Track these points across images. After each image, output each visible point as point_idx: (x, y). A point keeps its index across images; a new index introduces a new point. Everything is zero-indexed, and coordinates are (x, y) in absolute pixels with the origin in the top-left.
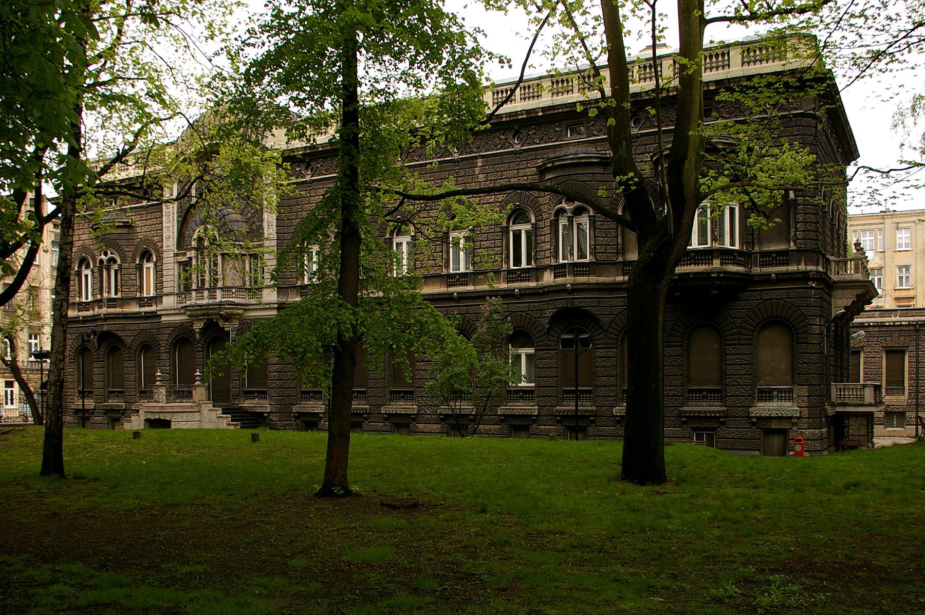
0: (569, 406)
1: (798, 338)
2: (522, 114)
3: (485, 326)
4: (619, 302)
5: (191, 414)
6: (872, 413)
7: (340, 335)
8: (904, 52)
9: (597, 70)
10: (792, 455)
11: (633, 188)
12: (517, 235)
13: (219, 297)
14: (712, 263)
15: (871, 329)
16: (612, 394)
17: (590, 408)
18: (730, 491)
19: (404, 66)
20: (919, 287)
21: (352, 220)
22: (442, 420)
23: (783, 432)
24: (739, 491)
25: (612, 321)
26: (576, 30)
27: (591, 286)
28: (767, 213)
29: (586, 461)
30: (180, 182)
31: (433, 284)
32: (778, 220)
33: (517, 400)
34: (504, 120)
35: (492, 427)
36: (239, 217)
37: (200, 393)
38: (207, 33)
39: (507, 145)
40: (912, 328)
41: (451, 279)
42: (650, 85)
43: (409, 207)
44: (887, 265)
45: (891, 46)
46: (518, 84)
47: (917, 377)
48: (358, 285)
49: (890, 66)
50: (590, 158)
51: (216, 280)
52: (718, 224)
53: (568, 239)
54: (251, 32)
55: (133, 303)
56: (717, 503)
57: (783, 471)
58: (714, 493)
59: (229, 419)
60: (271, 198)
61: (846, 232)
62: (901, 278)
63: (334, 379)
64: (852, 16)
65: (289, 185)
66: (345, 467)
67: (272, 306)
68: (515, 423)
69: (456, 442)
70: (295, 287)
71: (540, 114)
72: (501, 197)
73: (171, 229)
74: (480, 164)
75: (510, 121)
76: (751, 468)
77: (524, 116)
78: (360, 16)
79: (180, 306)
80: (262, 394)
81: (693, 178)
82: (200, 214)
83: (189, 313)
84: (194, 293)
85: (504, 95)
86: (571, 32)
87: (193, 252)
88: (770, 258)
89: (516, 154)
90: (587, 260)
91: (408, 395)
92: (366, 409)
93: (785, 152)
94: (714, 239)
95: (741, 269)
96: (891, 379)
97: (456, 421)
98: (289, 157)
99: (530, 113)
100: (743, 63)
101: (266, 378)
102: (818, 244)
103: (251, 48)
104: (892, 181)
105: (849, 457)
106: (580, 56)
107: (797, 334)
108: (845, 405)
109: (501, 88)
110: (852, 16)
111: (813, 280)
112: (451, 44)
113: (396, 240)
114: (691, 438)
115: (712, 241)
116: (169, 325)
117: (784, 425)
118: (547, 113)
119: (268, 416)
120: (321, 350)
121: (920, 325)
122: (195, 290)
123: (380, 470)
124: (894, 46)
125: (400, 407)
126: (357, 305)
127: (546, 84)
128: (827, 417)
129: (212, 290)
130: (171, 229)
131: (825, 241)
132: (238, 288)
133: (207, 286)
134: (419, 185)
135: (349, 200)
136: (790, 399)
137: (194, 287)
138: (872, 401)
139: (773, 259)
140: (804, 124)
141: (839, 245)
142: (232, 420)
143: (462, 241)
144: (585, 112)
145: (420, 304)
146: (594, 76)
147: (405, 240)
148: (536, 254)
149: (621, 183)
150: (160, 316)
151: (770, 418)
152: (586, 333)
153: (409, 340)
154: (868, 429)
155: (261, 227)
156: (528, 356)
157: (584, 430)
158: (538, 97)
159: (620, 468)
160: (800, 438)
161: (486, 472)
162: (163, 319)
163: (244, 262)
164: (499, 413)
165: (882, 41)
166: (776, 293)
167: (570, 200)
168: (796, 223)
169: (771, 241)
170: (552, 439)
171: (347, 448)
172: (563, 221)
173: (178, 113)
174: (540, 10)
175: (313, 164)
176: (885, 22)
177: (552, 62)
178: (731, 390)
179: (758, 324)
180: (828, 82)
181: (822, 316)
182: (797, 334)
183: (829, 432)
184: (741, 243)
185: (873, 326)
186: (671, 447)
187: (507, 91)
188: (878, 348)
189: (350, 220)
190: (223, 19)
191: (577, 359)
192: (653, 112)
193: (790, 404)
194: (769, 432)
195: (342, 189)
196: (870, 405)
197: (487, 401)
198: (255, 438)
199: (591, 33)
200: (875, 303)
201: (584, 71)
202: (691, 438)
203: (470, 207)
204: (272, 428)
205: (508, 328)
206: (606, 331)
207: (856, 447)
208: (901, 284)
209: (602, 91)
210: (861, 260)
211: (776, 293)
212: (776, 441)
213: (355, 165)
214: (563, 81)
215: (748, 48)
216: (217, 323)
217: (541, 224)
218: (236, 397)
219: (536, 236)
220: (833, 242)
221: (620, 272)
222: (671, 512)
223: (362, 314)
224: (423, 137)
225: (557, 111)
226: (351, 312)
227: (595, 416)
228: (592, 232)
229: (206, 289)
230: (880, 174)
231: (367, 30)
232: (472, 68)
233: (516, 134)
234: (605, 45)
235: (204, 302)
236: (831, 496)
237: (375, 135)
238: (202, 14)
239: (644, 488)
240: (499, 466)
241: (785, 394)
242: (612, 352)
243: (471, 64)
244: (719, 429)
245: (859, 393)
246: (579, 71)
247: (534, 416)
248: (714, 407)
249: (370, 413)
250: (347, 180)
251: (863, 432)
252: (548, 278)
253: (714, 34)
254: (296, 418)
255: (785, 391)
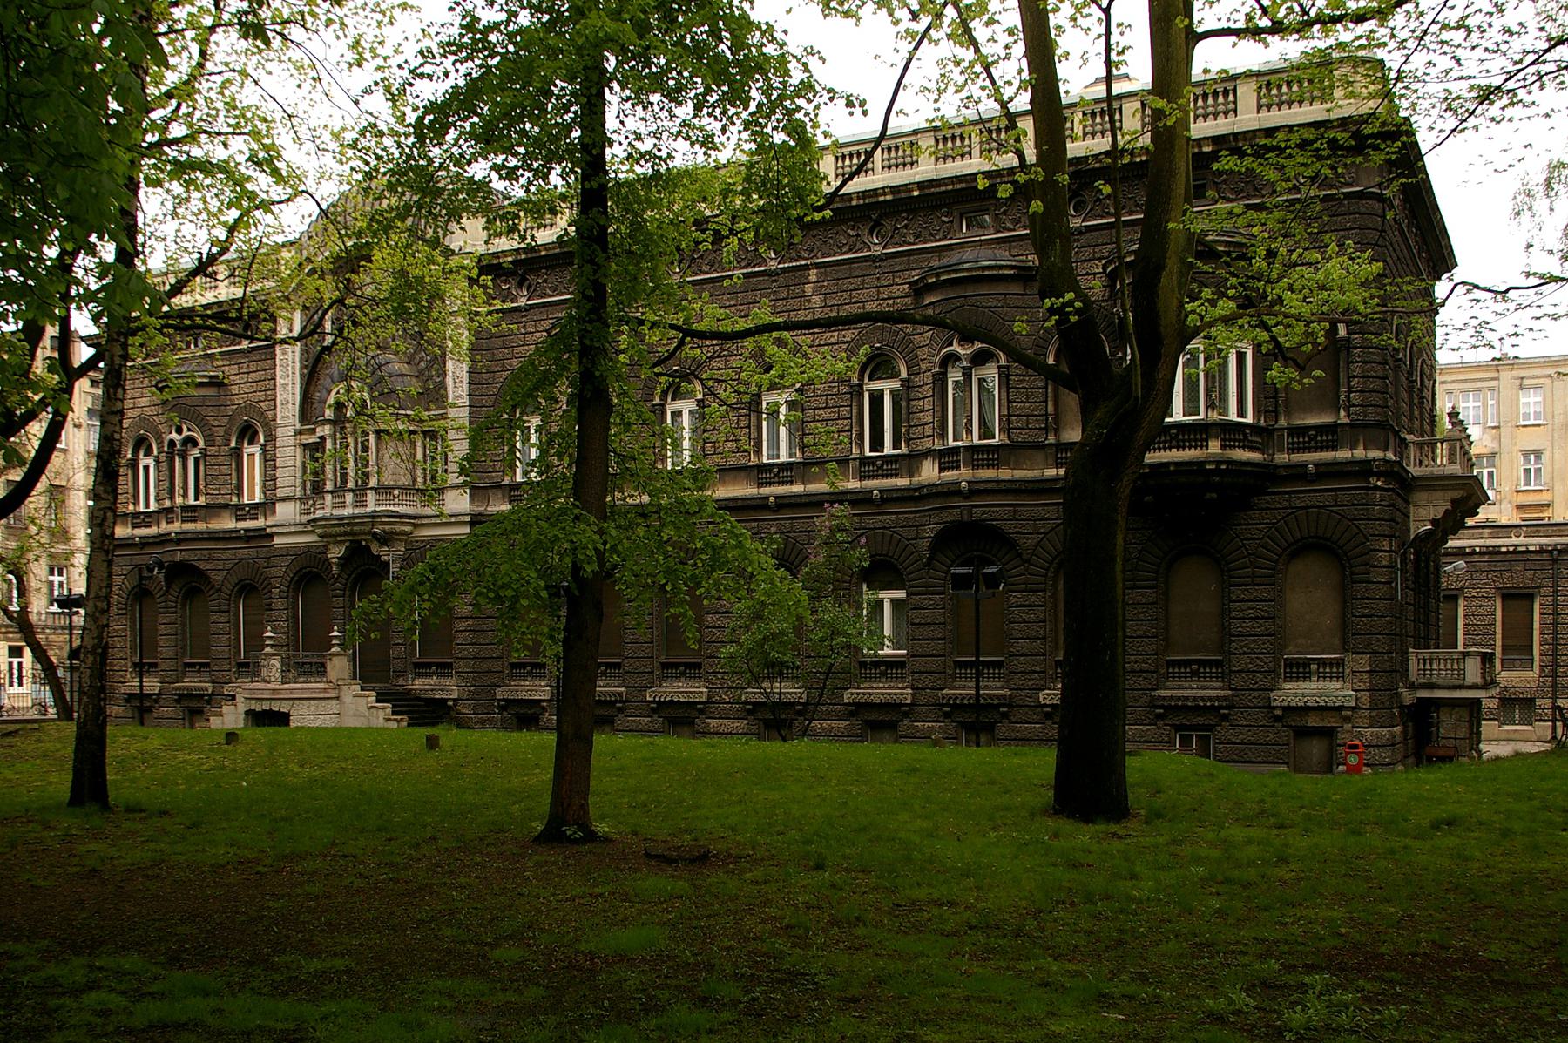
0: (964, 689)
1: (1352, 573)
2: (885, 194)
3: (823, 552)
4: (1049, 512)
5: (323, 703)
6: (1478, 701)
7: (576, 569)
8: (1532, 87)
9: (1012, 118)
10: (1343, 772)
11: (1073, 319)
12: (877, 399)
13: (372, 503)
14: (1207, 447)
15: (1476, 558)
16: (1037, 669)
17: (1000, 692)
18: (1237, 833)
19: (685, 111)
20: (1558, 487)
21: (597, 374)
22: (750, 712)
23: (1328, 733)
24: (1253, 832)
25: (1038, 544)
26: (977, 50)
27: (1002, 486)
28: (1300, 362)
29: (993, 782)
30: (305, 308)
31: (734, 481)
32: (1318, 373)
33: (876, 678)
34: (854, 203)
35: (833, 724)
36: (404, 368)
37: (338, 666)
38: (351, 56)
39: (859, 245)
40: (1545, 556)
41: (765, 474)
42: (1102, 144)
43: (693, 351)
44: (1504, 450)
45: (1510, 78)
46: (877, 142)
47: (1555, 639)
48: (607, 483)
49: (1509, 112)
50: (1001, 267)
51: (367, 475)
52: (1217, 380)
53: (962, 405)
54: (425, 54)
55: (226, 514)
56: (1216, 853)
57: (1328, 798)
58: (1211, 836)
59: (389, 711)
60: (459, 335)
61: (1434, 394)
62: (1527, 471)
63: (566, 642)
64: (1445, 27)
65: (489, 313)
66: (586, 792)
67: (462, 519)
68: (873, 718)
69: (774, 749)
70: (500, 487)
71: (916, 193)
72: (849, 335)
73: (290, 388)
74: (813, 278)
75: (865, 204)
76: (1274, 794)
77: (889, 197)
78: (610, 27)
79: (305, 519)
80: (445, 669)
81: (1175, 303)
82: (339, 363)
83: (320, 531)
84: (328, 497)
85: (855, 161)
86: (968, 54)
87: (327, 427)
88: (1305, 438)
89: (874, 261)
90: (995, 442)
91: (692, 670)
92: (620, 694)
93: (1330, 258)
94: (1210, 405)
95: (1256, 456)
96: (1510, 643)
97: (774, 714)
98: (490, 267)
99: (899, 192)
100: (1259, 108)
101: (451, 641)
102: (1386, 414)
103: (426, 81)
104: (1512, 306)
105: (1440, 775)
106: (984, 95)
107: (1351, 567)
108: (1432, 686)
109: (850, 149)
110: (1445, 27)
111: (1379, 475)
112: (765, 74)
113: (672, 407)
114: (1171, 743)
115: (1207, 408)
116: (287, 551)
117: (1330, 721)
118: (927, 191)
119: (455, 705)
120: (544, 594)
121: (1560, 551)
122: (331, 492)
123: (644, 797)
124: (1515, 78)
125: (678, 690)
126: (604, 518)
127: (926, 142)
128: (1402, 707)
129: (360, 491)
130: (290, 388)
131: (1399, 408)
132: (403, 489)
133: (351, 485)
134: (710, 314)
135: (592, 340)
136: (1340, 676)
137: (329, 486)
138: (1479, 680)
139: (1310, 440)
140: (1363, 210)
141: (1421, 416)
142: (394, 713)
143: (783, 409)
144: (992, 189)
145: (711, 516)
146: (1007, 129)
147: (686, 407)
148: (908, 431)
149: (1052, 311)
150: (271, 536)
151: (1306, 710)
152: (994, 564)
153: (694, 577)
154: (1471, 727)
155: (443, 385)
156: (894, 603)
157: (990, 729)
158: (912, 164)
159: (1051, 793)
160: (1356, 742)
161: (824, 800)
162: (277, 540)
163: (413, 444)
164: (846, 701)
165: (1495, 69)
166: (1316, 496)
167: (966, 339)
168: (1350, 378)
169: (1307, 410)
170: (935, 745)
171: (588, 759)
172: (954, 376)
173: (302, 192)
174: (915, 17)
175: (531, 278)
176: (1500, 38)
177: (936, 106)
178: (1239, 662)
179: (1284, 550)
180: (1404, 139)
181: (1393, 536)
182: (1351, 567)
183: (1405, 732)
184: (1256, 413)
185: (1480, 553)
186: (1138, 759)
187: (859, 154)
188: (1488, 590)
189: (593, 373)
190: (377, 32)
191: (977, 609)
192: (1107, 190)
193: (1338, 685)
194: (1303, 733)
195: (579, 320)
196: (1474, 687)
197: (826, 680)
198: (432, 743)
199: (1003, 56)
200: (1484, 513)
201: (990, 120)
202: (1171, 743)
203: (796, 350)
204: (461, 725)
205: (860, 557)
206: (1028, 561)
207: (1451, 759)
208: (1528, 482)
209: (1020, 154)
210: (1460, 441)
211: (1316, 496)
212: (1316, 748)
213: (602, 280)
214: (954, 138)
215: (1268, 81)
216: (367, 547)
217: (917, 380)
218: (401, 673)
219: (909, 400)
220: (1411, 410)
221: (1051, 461)
222: (1138, 869)
223: (614, 533)
224: (717, 232)
225: (943, 189)
226: (596, 529)
227: (1009, 706)
228: (1004, 394)
229: (350, 490)
230: (1492, 295)
231: (622, 52)
232: (800, 115)
233: (875, 227)
234: (1025, 75)
235: (346, 512)
236: (1409, 841)
237: (636, 230)
238: (342, 24)
239: (1092, 828)
240: (845, 791)
241: (1331, 668)
242: (1037, 598)
243: (799, 109)
244: (1219, 728)
245: (1456, 667)
246: (982, 121)
247: (906, 705)
248: (1210, 690)
249: (627, 701)
250: (589, 306)
251: (1463, 732)
252: (929, 472)
253: (1210, 58)
254: (502, 708)
255: (1331, 663)
